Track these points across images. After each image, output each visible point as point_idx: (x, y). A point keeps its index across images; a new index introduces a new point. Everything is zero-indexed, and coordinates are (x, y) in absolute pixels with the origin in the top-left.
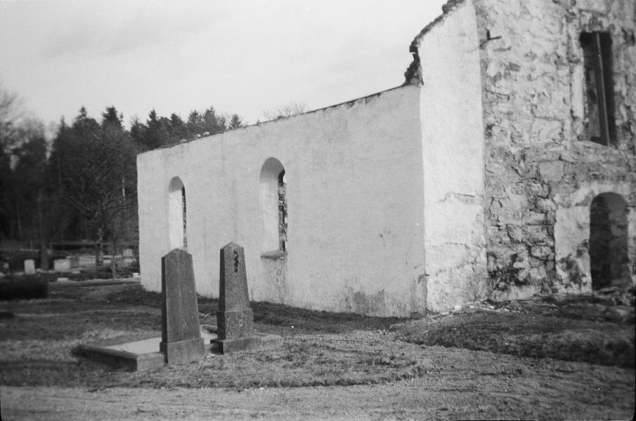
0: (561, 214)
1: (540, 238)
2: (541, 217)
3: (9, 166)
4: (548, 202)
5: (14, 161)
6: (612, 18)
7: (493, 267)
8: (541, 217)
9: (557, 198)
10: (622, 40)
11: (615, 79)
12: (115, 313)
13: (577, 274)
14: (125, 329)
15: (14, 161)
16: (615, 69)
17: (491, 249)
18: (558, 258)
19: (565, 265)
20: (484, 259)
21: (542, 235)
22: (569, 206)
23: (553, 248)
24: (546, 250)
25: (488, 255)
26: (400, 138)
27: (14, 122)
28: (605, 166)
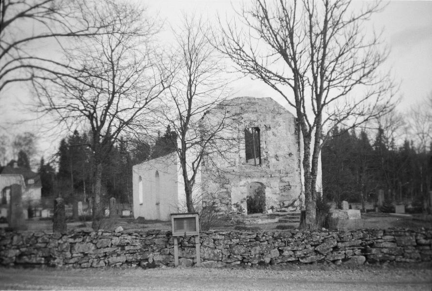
0: (233, 189)
1: (225, 197)
2: (225, 190)
3: (409, 147)
4: (229, 185)
5: (374, 148)
6: (260, 122)
7: (204, 205)
8: (225, 190)
9: (232, 184)
10: (264, 129)
11: (261, 143)
12: (74, 178)
13: (241, 209)
14: (33, 203)
15: (374, 148)
16: (261, 139)
17: (204, 200)
18: (233, 203)
19: (235, 206)
20: (201, 202)
21: (226, 196)
22: (237, 186)
23: (230, 200)
24: (228, 201)
25: (203, 202)
26: (208, 112)
27: (77, 129)
28: (254, 173)
